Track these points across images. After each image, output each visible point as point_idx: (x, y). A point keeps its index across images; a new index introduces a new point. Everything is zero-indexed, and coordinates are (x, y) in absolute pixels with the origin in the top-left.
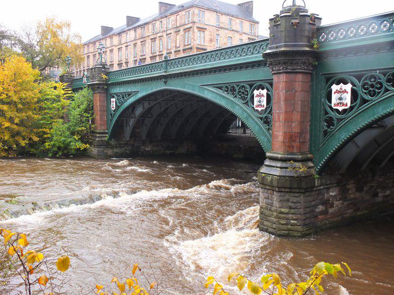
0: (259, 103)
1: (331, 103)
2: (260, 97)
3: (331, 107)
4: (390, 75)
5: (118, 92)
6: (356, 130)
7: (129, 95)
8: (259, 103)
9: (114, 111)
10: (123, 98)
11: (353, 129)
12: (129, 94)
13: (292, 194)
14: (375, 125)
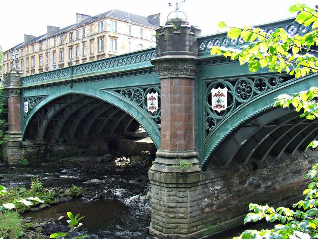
0: (151, 106)
1: (211, 105)
2: (152, 100)
3: (211, 109)
4: (239, 82)
5: (31, 95)
6: (232, 130)
7: (40, 98)
8: (151, 106)
9: (27, 113)
10: (35, 101)
11: (230, 128)
12: (41, 98)
13: (179, 190)
14: (248, 125)
